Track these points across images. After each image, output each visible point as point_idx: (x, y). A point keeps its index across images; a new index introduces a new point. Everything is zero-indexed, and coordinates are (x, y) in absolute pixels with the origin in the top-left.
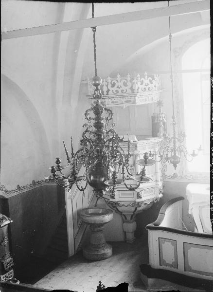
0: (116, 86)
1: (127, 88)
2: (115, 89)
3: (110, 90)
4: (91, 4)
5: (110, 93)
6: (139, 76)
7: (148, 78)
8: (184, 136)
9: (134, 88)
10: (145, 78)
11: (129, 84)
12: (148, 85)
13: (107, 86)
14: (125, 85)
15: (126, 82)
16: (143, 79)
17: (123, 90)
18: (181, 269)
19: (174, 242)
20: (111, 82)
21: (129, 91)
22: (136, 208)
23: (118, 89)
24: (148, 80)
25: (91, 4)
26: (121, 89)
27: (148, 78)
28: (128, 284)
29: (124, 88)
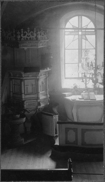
0: (26, 35)
1: (33, 37)
2: (26, 37)
3: (22, 38)
4: (78, 17)
5: (22, 39)
6: (22, 30)
7: (30, 32)
8: (98, 80)
9: (38, 37)
10: (27, 32)
11: (35, 35)
12: (30, 36)
13: (20, 35)
14: (33, 35)
15: (33, 33)
16: (26, 32)
17: (31, 38)
18: (79, 144)
19: (75, 130)
20: (23, 32)
21: (35, 39)
22: (37, 106)
23: (27, 37)
24: (43, 33)
25: (90, 21)
26: (30, 37)
27: (30, 32)
28: (2, 181)
29: (31, 37)
